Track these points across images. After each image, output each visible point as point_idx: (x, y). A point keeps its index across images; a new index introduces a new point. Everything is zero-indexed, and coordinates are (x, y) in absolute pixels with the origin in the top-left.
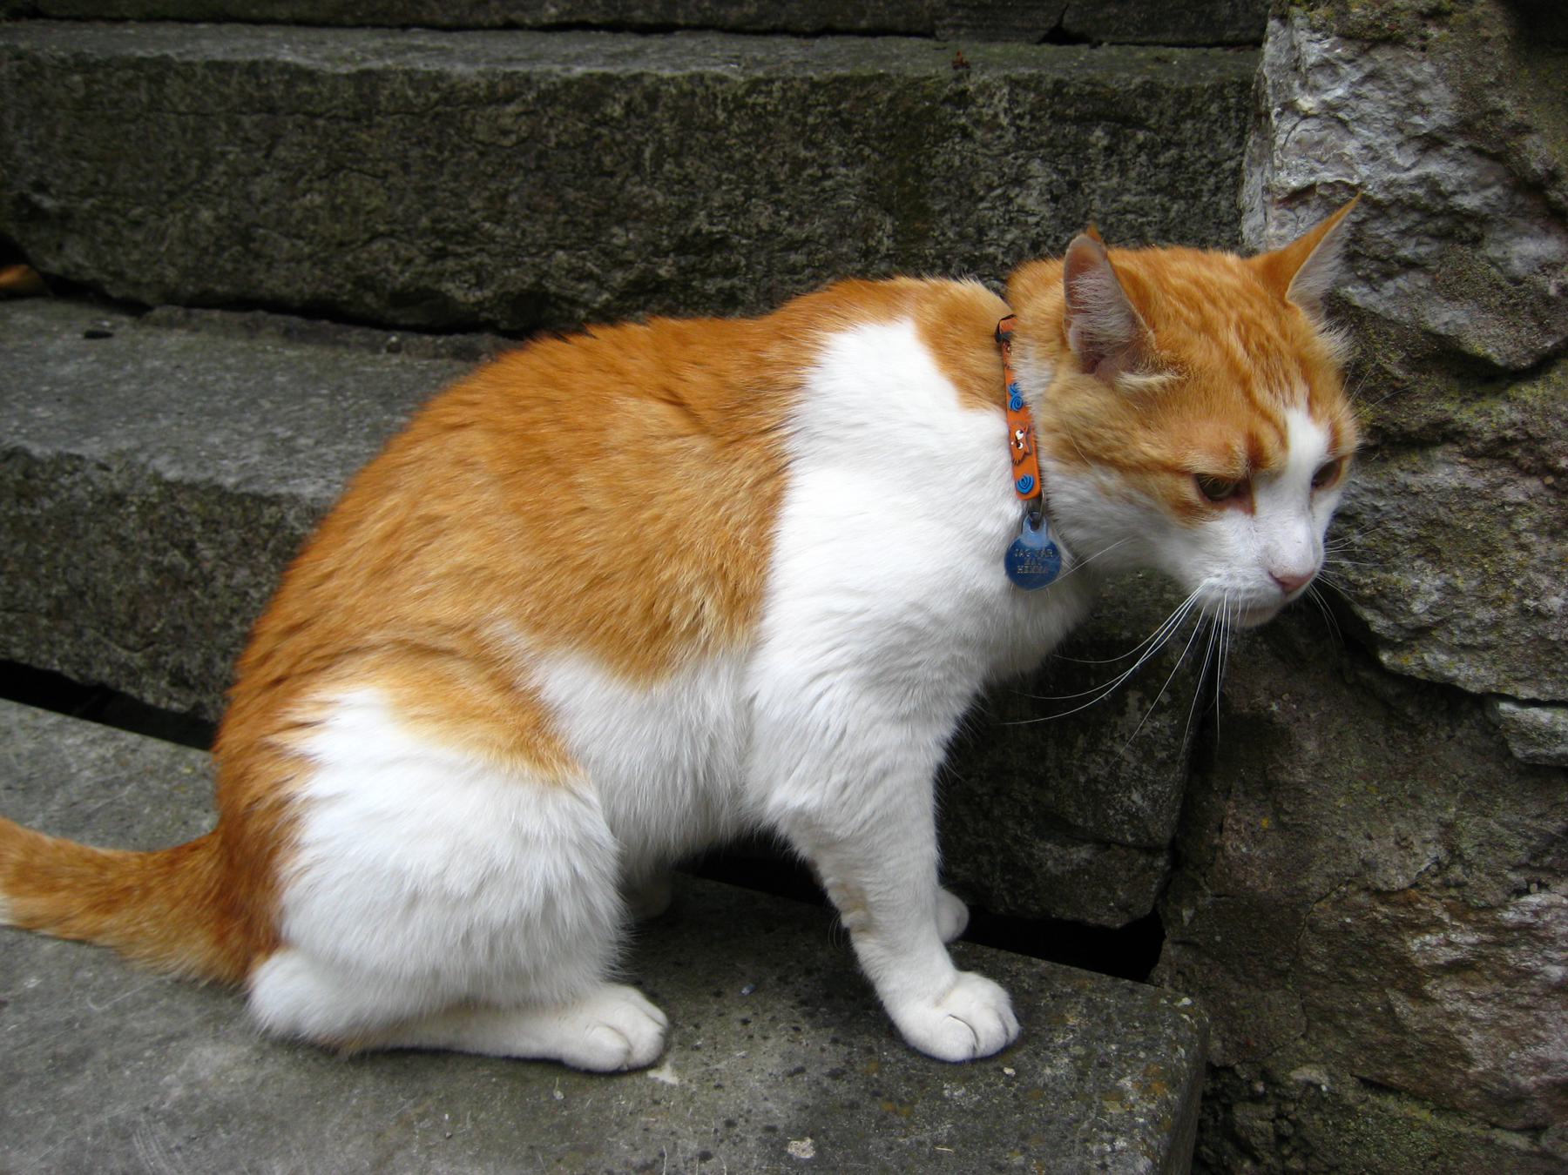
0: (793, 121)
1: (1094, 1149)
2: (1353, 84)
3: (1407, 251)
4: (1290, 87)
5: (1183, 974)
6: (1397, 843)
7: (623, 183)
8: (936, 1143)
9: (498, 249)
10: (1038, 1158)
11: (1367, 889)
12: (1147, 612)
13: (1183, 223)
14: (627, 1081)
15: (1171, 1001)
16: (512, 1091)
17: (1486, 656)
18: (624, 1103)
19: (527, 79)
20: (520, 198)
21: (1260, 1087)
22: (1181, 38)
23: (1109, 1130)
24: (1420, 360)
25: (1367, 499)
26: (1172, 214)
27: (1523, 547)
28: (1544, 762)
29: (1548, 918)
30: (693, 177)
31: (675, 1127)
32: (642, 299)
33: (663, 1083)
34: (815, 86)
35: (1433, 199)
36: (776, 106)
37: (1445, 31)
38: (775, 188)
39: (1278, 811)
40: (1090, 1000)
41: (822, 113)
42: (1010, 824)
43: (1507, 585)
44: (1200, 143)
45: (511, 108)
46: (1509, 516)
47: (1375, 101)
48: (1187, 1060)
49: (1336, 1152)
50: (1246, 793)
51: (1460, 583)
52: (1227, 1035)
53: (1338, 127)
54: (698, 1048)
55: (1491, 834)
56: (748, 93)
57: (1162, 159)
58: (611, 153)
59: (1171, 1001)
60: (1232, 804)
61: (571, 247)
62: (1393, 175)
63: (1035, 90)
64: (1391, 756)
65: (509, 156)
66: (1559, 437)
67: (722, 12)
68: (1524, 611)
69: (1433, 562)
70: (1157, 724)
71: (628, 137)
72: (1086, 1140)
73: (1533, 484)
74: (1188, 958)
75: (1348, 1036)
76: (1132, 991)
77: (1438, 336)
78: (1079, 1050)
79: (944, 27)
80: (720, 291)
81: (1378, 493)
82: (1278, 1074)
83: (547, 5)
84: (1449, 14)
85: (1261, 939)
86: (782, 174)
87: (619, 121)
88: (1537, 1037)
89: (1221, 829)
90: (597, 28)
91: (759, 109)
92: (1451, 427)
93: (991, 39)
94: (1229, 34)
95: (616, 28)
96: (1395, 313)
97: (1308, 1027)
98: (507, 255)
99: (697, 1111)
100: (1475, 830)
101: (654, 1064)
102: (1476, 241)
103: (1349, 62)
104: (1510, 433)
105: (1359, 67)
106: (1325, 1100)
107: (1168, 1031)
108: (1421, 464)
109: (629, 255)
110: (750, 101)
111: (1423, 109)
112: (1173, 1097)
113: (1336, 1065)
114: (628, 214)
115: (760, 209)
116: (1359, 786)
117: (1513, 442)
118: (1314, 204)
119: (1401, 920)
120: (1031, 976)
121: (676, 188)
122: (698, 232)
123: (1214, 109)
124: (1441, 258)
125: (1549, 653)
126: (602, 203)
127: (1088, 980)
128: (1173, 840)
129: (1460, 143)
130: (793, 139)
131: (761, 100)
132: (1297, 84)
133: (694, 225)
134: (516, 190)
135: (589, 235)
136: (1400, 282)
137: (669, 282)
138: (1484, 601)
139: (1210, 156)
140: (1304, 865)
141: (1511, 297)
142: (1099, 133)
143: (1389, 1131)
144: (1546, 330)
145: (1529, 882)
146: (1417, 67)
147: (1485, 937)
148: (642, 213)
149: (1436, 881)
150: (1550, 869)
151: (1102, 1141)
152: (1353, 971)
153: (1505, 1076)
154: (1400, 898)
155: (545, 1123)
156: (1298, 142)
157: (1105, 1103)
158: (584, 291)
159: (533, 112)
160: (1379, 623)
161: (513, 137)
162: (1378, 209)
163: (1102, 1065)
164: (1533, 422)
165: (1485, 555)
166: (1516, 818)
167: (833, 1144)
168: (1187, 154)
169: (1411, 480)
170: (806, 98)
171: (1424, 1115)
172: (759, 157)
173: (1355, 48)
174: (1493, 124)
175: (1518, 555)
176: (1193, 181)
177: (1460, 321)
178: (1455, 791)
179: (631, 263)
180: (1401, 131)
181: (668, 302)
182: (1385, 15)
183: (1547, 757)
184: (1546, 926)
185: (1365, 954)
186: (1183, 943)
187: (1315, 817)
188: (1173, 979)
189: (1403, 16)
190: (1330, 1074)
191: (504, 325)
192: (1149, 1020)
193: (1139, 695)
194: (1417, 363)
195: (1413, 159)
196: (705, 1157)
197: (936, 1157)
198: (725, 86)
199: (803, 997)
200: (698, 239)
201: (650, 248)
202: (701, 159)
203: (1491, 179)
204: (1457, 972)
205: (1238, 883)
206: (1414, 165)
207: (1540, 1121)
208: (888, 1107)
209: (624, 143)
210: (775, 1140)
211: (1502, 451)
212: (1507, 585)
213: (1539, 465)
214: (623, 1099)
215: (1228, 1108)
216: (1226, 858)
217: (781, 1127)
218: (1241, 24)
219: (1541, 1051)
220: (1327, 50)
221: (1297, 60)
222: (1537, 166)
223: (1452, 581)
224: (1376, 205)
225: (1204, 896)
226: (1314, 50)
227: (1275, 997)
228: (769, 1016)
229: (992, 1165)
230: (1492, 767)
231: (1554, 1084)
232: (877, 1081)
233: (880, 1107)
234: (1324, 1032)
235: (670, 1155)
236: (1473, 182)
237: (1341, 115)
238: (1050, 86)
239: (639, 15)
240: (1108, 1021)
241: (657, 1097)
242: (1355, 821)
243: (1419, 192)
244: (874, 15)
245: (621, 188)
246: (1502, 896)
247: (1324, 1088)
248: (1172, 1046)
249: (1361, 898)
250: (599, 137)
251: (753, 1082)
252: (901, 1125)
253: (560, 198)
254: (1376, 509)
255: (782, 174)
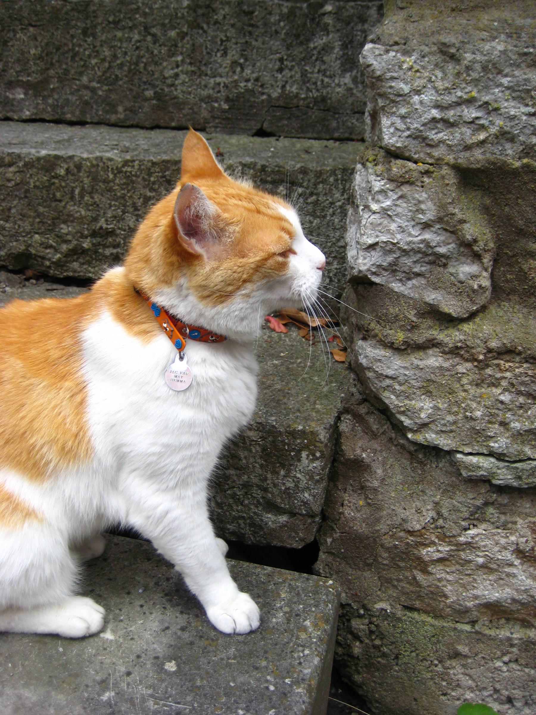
0: (144, 179)
1: (296, 655)
2: (394, 200)
3: (416, 270)
4: (367, 199)
5: (328, 566)
6: (416, 511)
7: (66, 205)
8: (229, 659)
9: (7, 233)
10: (273, 662)
11: (404, 530)
12: (309, 415)
13: (319, 228)
14: (91, 640)
15: (324, 583)
16: (39, 649)
17: (451, 435)
18: (90, 650)
19: (19, 156)
20: (17, 210)
21: (362, 612)
22: (315, 135)
23: (302, 646)
24: (423, 314)
25: (402, 371)
26: (314, 224)
27: (465, 391)
28: (475, 478)
29: (477, 539)
30: (98, 203)
31: (114, 660)
32: (75, 257)
33: (107, 639)
34: (154, 164)
35: (427, 248)
36: (136, 172)
37: (431, 180)
38: (136, 209)
39: (367, 498)
40: (290, 584)
41: (157, 176)
42: (252, 507)
43: (459, 406)
44: (326, 194)
45: (12, 169)
46: (460, 378)
47: (403, 207)
48: (332, 609)
49: (394, 636)
50: (353, 490)
51: (440, 405)
52: (347, 591)
53: (388, 217)
54: (121, 621)
55: (454, 506)
56: (123, 166)
57: (309, 200)
58: (60, 191)
59: (324, 583)
60: (347, 495)
61: (42, 233)
62: (411, 239)
63: (253, 168)
64: (413, 475)
65: (11, 191)
66: (479, 347)
67: (108, 117)
68: (466, 417)
69: (429, 396)
70: (315, 465)
71: (67, 184)
72: (292, 652)
73: (469, 365)
74: (330, 559)
75: (398, 589)
76: (308, 579)
77: (430, 304)
78: (286, 609)
79: (210, 127)
80: (112, 254)
81: (404, 368)
82: (369, 606)
83: (25, 110)
84: (432, 172)
85: (361, 550)
86: (140, 202)
87: (63, 177)
88: (473, 586)
89: (342, 505)
90: (49, 121)
91: (128, 174)
92: (436, 341)
93: (231, 133)
94: (336, 135)
95: (58, 122)
96: (412, 295)
97: (381, 586)
98: (12, 236)
99: (123, 652)
100: (447, 505)
101: (103, 630)
102: (445, 265)
103: (392, 191)
104: (459, 344)
105: (396, 193)
106: (389, 616)
107: (324, 597)
108: (424, 356)
109: (69, 237)
110: (124, 170)
111: (423, 212)
112: (327, 627)
113: (393, 601)
114: (69, 219)
115: (130, 218)
116: (400, 487)
117: (461, 348)
118: (378, 250)
119: (418, 542)
120: (264, 575)
121: (91, 208)
122: (101, 228)
123: (332, 179)
124: (431, 272)
125: (476, 434)
126: (56, 214)
127: (289, 575)
128: (322, 510)
129: (438, 226)
130: (144, 187)
131: (129, 169)
132: (370, 198)
133: (99, 225)
134: (15, 207)
135: (50, 228)
136: (414, 281)
137: (88, 250)
138: (450, 413)
139: (330, 200)
140: (378, 520)
141: (459, 289)
142: (281, 188)
143: (415, 627)
144: (473, 302)
145: (469, 525)
146: (420, 194)
147: (453, 548)
148: (75, 218)
149: (432, 526)
150: (478, 519)
151: (299, 651)
152: (399, 563)
153: (462, 603)
154: (418, 533)
155: (56, 663)
156: (371, 224)
157: (299, 633)
158: (48, 253)
159: (22, 171)
160: (407, 422)
161: (13, 183)
162: (405, 252)
163: (297, 615)
164: (469, 340)
165: (450, 394)
166: (464, 500)
167: (184, 663)
168: (320, 199)
169: (420, 363)
170: (150, 169)
171: (429, 619)
172: (129, 195)
173: (394, 185)
174: (451, 219)
175: (463, 394)
176: (323, 210)
177: (439, 299)
178: (439, 489)
179: (70, 241)
180: (414, 220)
181: (88, 258)
182: (406, 172)
183: (476, 476)
184: (476, 542)
185: (404, 556)
186: (327, 552)
187: (382, 501)
188: (324, 568)
189: (414, 173)
190: (391, 605)
191: (11, 267)
192: (316, 593)
193: (307, 453)
194: (421, 315)
195: (419, 232)
196: (129, 674)
197: (229, 665)
198: (112, 163)
199: (166, 592)
200: (101, 231)
201: (79, 235)
202: (102, 195)
203: (451, 241)
204: (441, 562)
205: (350, 528)
206: (419, 235)
207: (475, 619)
208: (207, 642)
209: (66, 187)
210: (159, 662)
211: (456, 352)
212: (459, 406)
213: (471, 357)
214: (90, 649)
215: (349, 621)
216: (345, 518)
217: (161, 656)
218: (341, 130)
219: (475, 592)
220: (383, 185)
221: (370, 188)
222: (469, 237)
223: (437, 404)
224: (404, 251)
225: (336, 533)
226: (378, 185)
227: (367, 574)
228: (152, 602)
229: (253, 667)
230: (454, 479)
231: (481, 605)
232: (201, 630)
233: (203, 643)
234: (388, 587)
235: (113, 675)
236: (443, 242)
237: (389, 213)
238: (260, 167)
239: (69, 116)
240: (298, 594)
241: (105, 647)
242: (398, 502)
243: (421, 246)
244: (178, 120)
245: (64, 207)
246: (459, 531)
247: (388, 611)
248: (326, 603)
249: (402, 534)
250: (54, 184)
251: (147, 635)
252: (213, 651)
253: (36, 211)
254: (405, 375)
255: (140, 202)
